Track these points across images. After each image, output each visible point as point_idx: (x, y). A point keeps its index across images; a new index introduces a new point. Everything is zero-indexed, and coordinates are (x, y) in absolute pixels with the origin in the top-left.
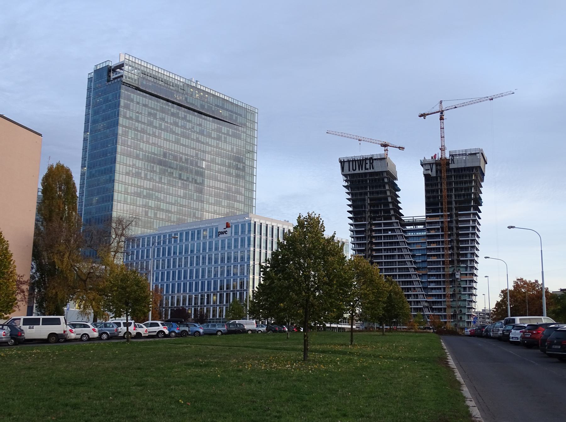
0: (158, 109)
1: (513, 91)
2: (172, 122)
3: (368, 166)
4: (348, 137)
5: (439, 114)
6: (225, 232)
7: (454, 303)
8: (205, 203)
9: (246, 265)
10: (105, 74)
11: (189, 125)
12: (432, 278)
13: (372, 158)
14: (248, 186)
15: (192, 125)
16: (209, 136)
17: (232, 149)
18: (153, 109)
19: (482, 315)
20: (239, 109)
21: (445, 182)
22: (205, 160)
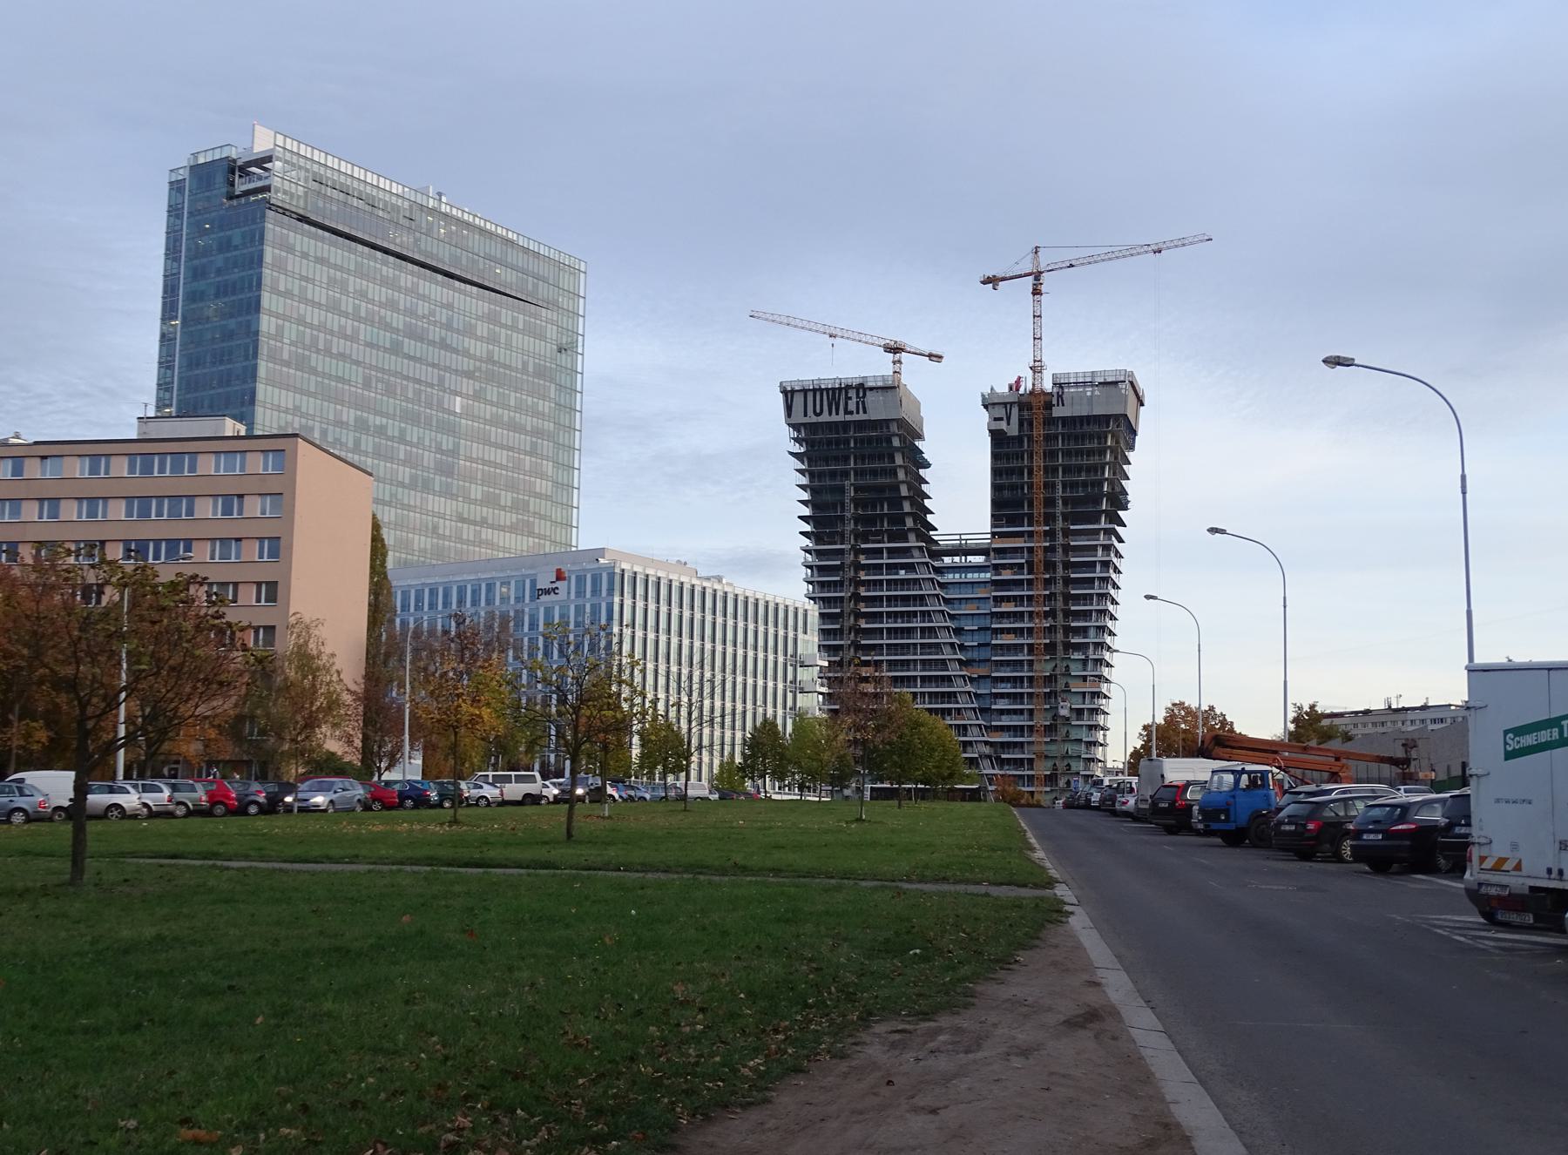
1: (1210, 234)
2: (384, 300)
3: (852, 406)
4: (803, 328)
5: (1031, 278)
6: (554, 590)
7: (1053, 747)
10: (220, 179)
11: (424, 307)
12: (1003, 685)
17: (525, 364)
20: (541, 263)
21: (1039, 449)
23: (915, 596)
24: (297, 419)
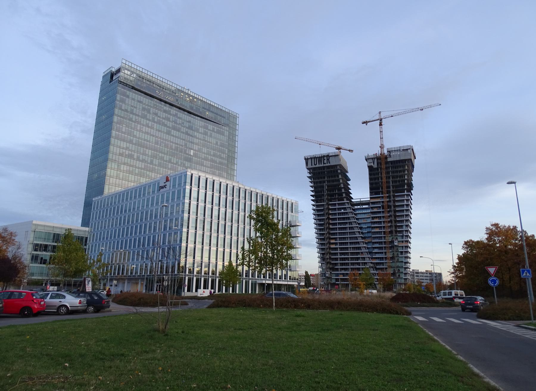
5: (379, 121)
6: (165, 186)
12: (376, 244)
19: (413, 273)
21: (384, 171)
22: (193, 149)
23: (347, 217)
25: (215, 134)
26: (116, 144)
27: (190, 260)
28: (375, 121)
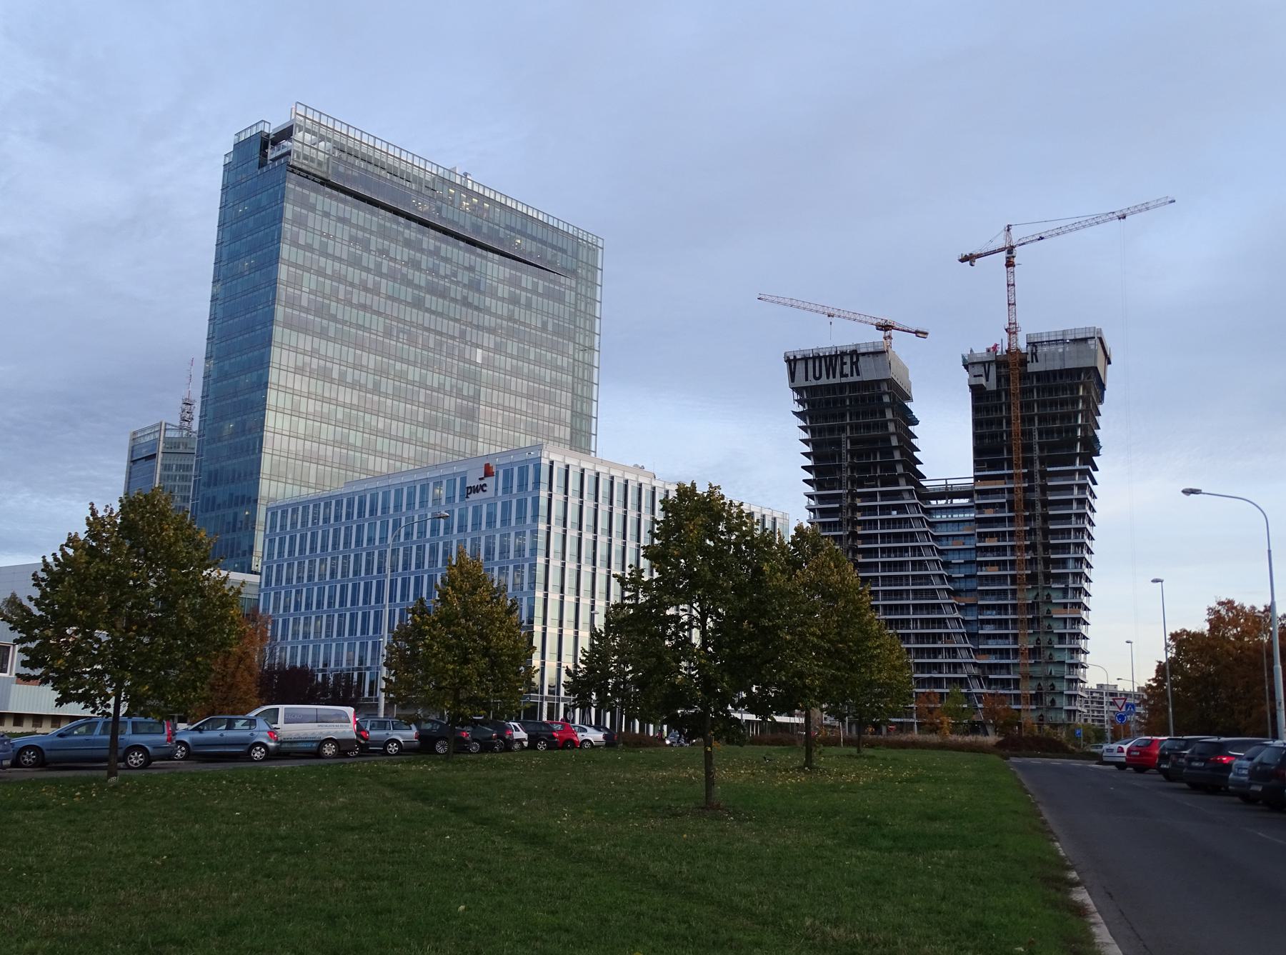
0: (374, 229)
5: (1004, 254)
8: (480, 440)
9: (527, 566)
11: (444, 269)
12: (989, 612)
13: (856, 351)
14: (579, 406)
15: (453, 268)
16: (493, 295)
17: (545, 324)
18: (363, 229)
19: (1098, 695)
21: (1016, 402)
22: (482, 347)
23: (906, 533)
24: (315, 360)
25: (540, 299)
26: (286, 340)
27: (551, 664)
28: (995, 252)
